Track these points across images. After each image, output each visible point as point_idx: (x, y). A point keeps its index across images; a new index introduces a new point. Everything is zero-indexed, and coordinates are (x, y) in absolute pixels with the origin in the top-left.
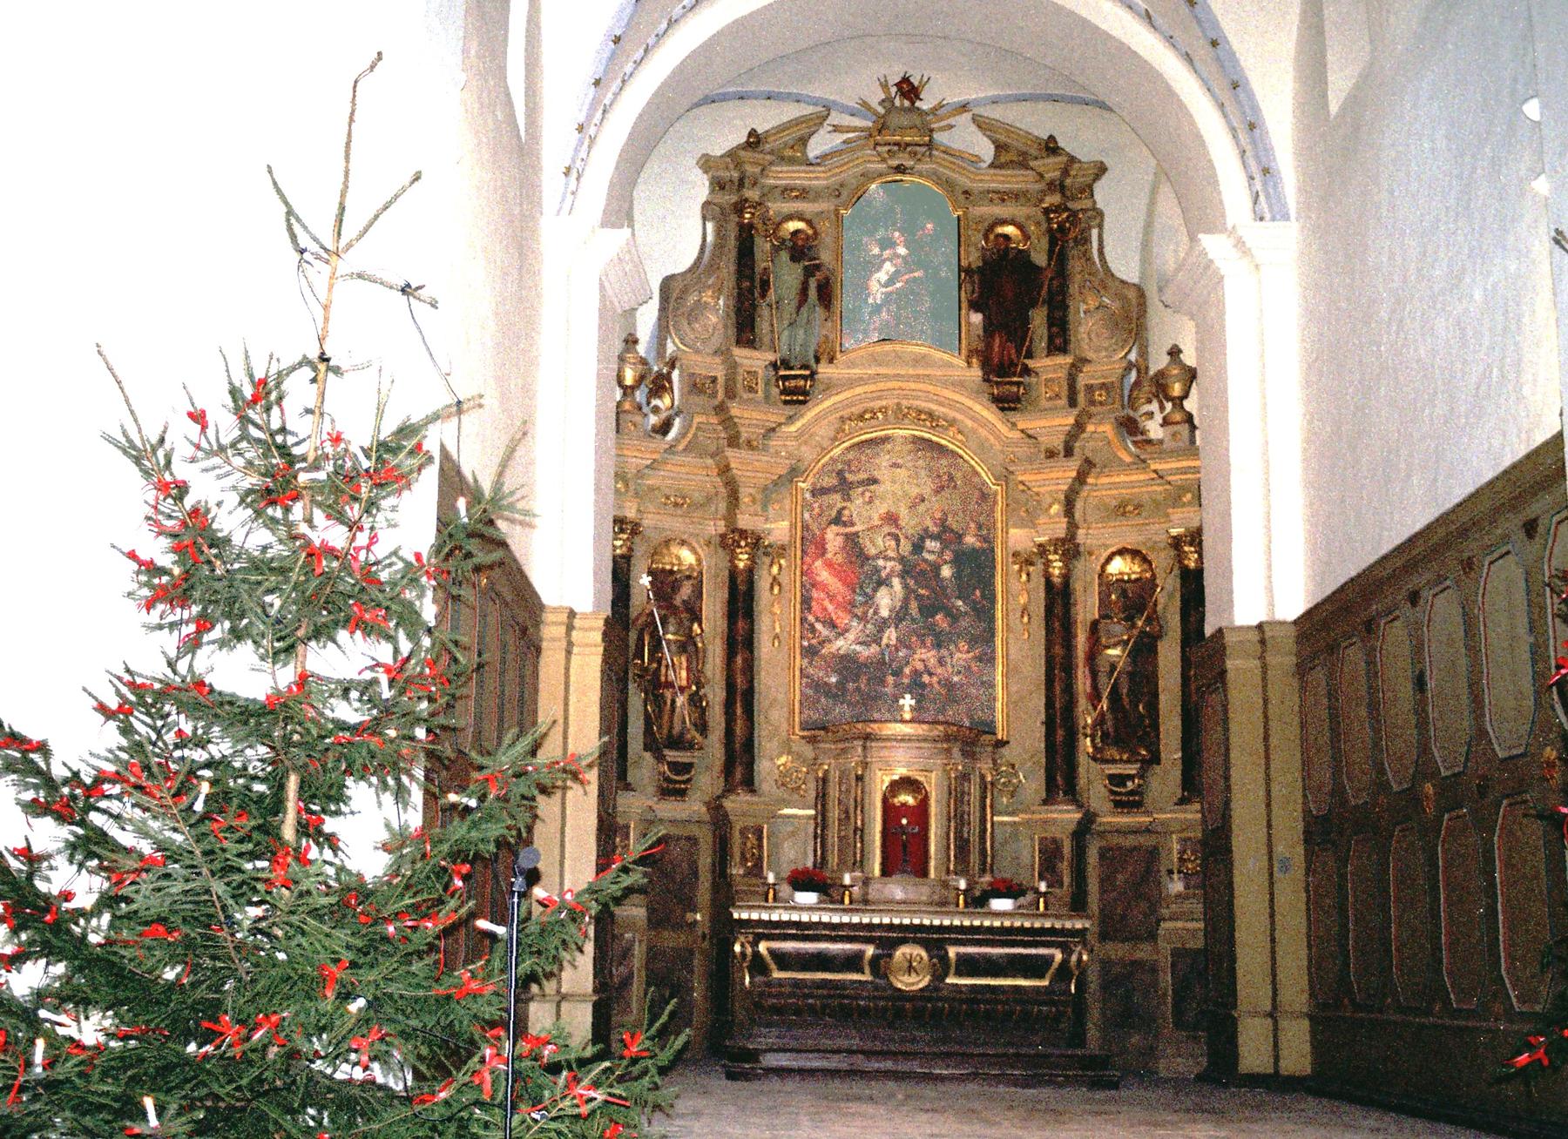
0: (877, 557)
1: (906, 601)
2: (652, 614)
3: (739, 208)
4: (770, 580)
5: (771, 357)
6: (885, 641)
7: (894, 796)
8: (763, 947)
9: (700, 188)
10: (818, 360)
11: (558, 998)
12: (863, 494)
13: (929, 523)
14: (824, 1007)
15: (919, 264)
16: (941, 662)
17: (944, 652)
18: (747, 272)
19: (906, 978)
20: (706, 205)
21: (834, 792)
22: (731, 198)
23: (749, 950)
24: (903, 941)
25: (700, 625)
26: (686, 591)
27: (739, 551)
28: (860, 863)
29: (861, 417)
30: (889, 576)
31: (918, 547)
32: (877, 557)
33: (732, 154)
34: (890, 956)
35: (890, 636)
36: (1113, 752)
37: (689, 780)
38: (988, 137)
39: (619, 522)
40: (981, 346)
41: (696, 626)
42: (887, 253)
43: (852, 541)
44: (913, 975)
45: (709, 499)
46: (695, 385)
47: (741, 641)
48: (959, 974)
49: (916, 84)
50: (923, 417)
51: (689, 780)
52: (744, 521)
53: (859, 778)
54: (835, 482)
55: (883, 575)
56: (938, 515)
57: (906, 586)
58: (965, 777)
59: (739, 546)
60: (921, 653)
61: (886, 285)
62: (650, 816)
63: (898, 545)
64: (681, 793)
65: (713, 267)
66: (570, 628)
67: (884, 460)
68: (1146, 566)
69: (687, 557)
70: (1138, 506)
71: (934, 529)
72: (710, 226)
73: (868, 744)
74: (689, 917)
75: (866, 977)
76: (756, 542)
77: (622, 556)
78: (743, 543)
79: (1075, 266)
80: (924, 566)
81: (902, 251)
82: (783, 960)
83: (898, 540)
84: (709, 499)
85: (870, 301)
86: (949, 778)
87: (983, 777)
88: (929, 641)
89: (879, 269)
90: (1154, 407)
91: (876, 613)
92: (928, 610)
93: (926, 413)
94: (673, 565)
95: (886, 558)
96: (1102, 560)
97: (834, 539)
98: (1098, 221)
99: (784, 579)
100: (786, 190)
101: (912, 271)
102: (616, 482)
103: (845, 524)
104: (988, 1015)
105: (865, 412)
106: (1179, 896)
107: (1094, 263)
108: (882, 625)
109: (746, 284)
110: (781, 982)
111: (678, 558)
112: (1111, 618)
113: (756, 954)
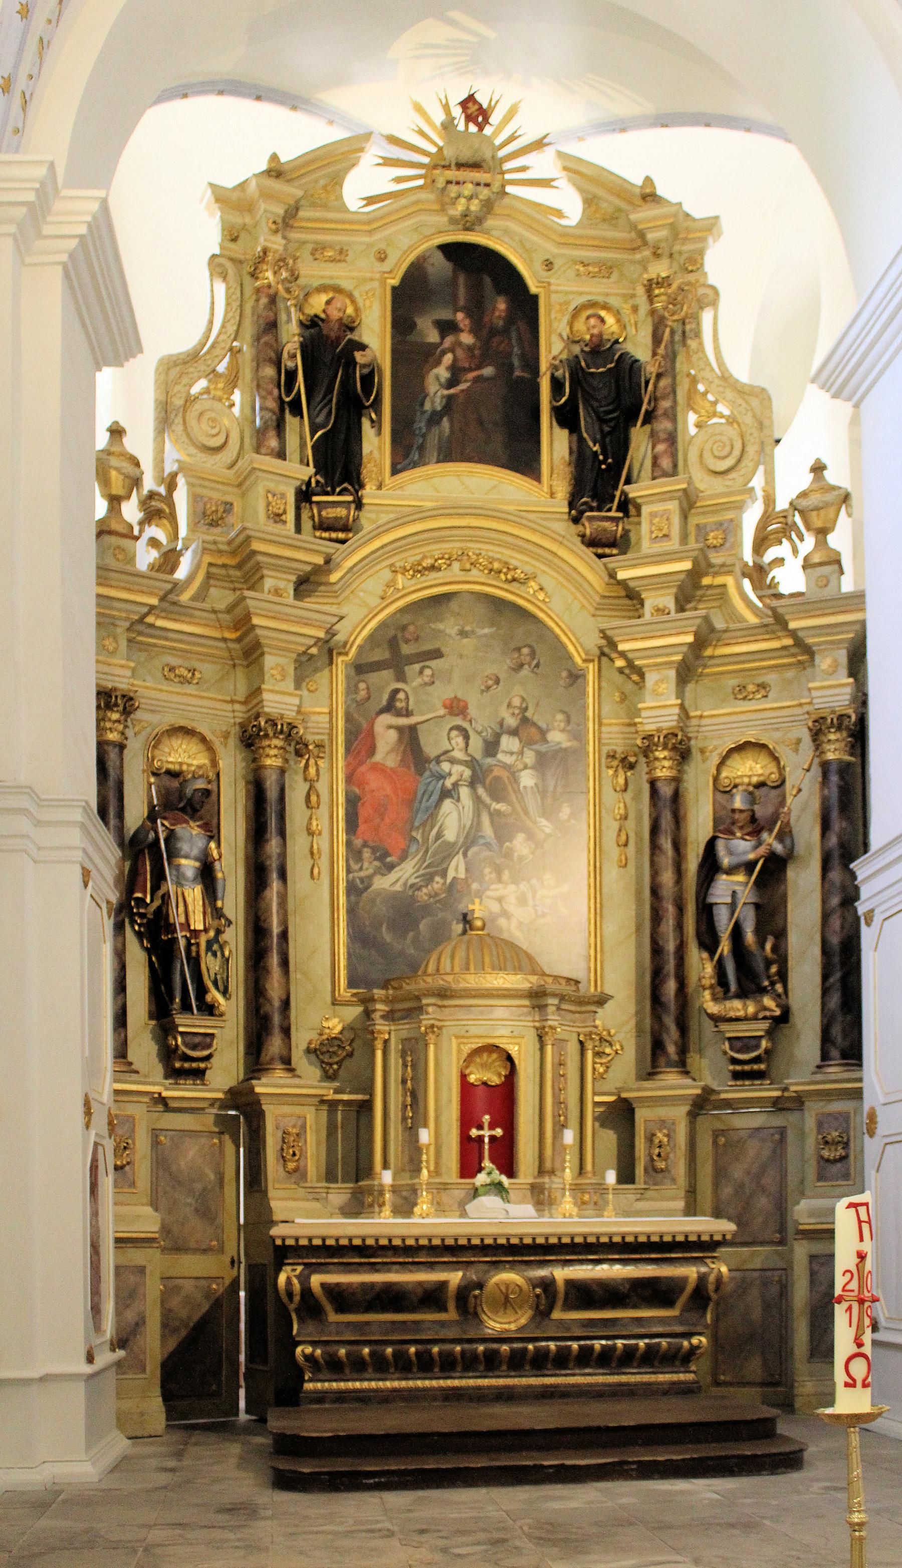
8: (316, 1280)
12: (421, 672)
17: (523, 886)
23: (297, 1286)
25: (219, 846)
30: (455, 785)
37: (208, 1058)
41: (213, 845)
42: (449, 341)
48: (569, 1306)
49: (485, 106)
51: (208, 1058)
54: (387, 655)
55: (449, 783)
57: (477, 799)
67: (449, 626)
81: (467, 339)
82: (338, 1295)
83: (467, 737)
85: (427, 406)
89: (438, 363)
91: (439, 836)
95: (453, 761)
101: (479, 367)
103: (398, 714)
113: (307, 1292)
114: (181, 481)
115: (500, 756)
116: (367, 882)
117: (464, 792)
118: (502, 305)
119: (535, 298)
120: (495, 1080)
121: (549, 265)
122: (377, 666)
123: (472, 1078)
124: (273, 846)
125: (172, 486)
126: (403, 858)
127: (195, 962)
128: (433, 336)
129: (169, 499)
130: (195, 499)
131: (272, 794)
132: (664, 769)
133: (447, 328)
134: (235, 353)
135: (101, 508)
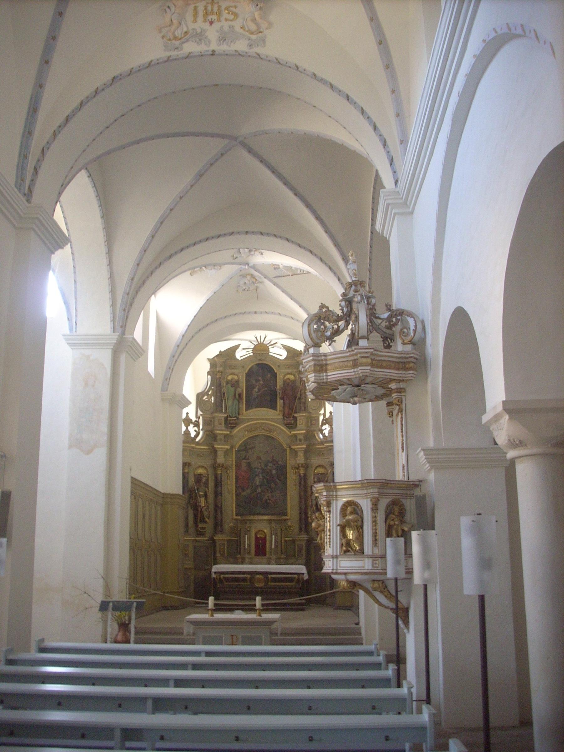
13: (269, 458)
30: (259, 473)
31: (266, 465)
35: (259, 490)
43: (249, 464)
47: (217, 494)
55: (257, 473)
81: (261, 382)
89: (255, 388)
95: (258, 469)
113: (220, 578)
114: (201, 417)
115: (268, 467)
116: (240, 493)
117: (261, 475)
118: (269, 375)
119: (276, 373)
120: (263, 536)
121: (279, 366)
122: (242, 451)
123: (258, 536)
124: (219, 489)
125: (199, 418)
126: (248, 488)
127: (201, 512)
128: (254, 382)
129: (198, 422)
130: (204, 420)
131: (219, 477)
132: (302, 471)
133: (257, 381)
134: (212, 389)
135: (184, 428)
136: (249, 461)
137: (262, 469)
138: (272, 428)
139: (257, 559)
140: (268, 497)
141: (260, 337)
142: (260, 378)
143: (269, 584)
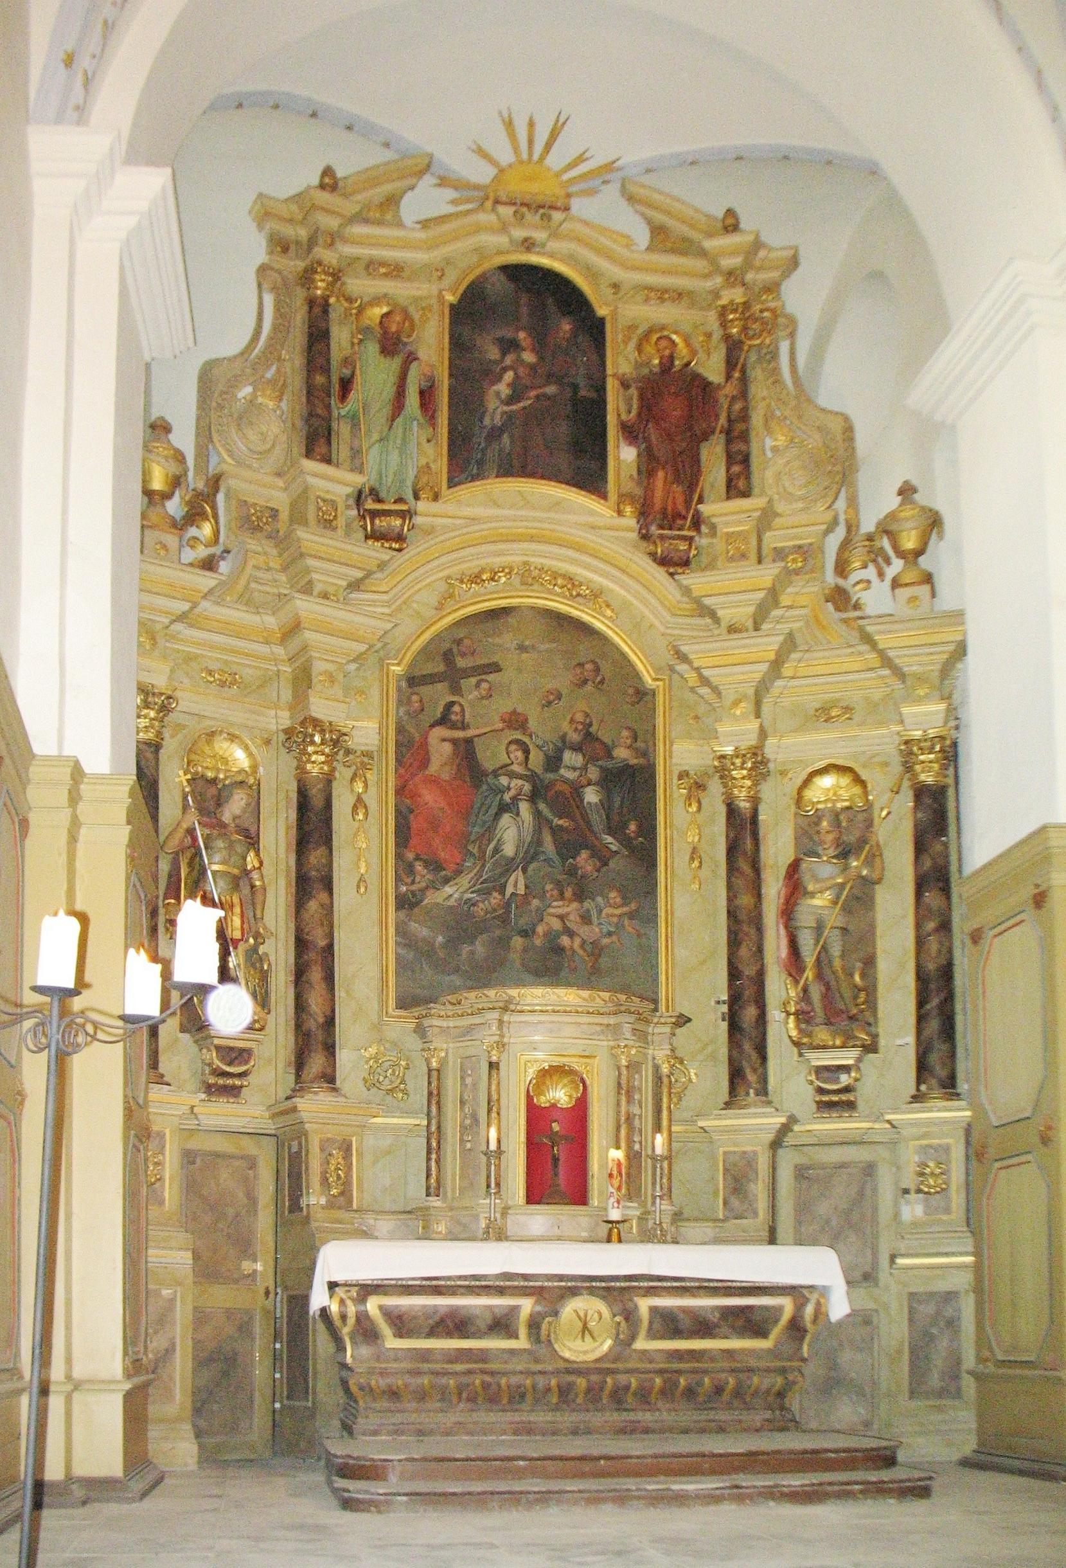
0: (496, 773)
1: (538, 831)
2: (191, 832)
3: (307, 277)
4: (352, 800)
5: (358, 480)
6: (510, 890)
7: (541, 1093)
8: (373, 1305)
9: (257, 250)
10: (417, 497)
11: (70, 1387)
12: (478, 685)
13: (566, 726)
14: (460, 1390)
15: (550, 378)
16: (586, 919)
18: (321, 361)
19: (578, 1344)
20: (262, 270)
21: (452, 1088)
22: (294, 265)
23: (351, 1309)
24: (574, 1292)
26: (236, 805)
27: (310, 749)
28: (495, 1185)
29: (476, 579)
30: (515, 799)
31: (553, 762)
32: (496, 773)
33: (297, 198)
34: (556, 1314)
35: (516, 883)
36: (822, 1034)
38: (642, 215)
39: (145, 691)
40: (638, 491)
43: (466, 752)
44: (588, 1337)
45: (265, 682)
46: (248, 518)
48: (652, 1335)
50: (560, 581)
52: (320, 707)
53: (493, 1066)
54: (441, 668)
55: (507, 797)
56: (579, 717)
57: (537, 814)
58: (634, 1066)
59: (313, 743)
60: (558, 907)
61: (510, 401)
62: (191, 1124)
63: (527, 759)
64: (233, 1092)
65: (272, 352)
66: (74, 798)
67: (508, 640)
68: (857, 790)
69: (240, 757)
70: (848, 709)
71: (574, 737)
72: (269, 300)
73: (506, 1018)
74: (247, 1266)
75: (522, 1342)
76: (337, 741)
77: (148, 743)
78: (317, 739)
79: (759, 390)
80: (559, 787)
81: (529, 357)
82: (401, 1324)
83: (527, 752)
84: (265, 682)
85: (487, 421)
86: (619, 1068)
87: (656, 1068)
88: (568, 893)
89: (499, 379)
90: (871, 572)
91: (497, 850)
92: (568, 848)
93: (564, 576)
94: (218, 770)
95: (512, 775)
96: (799, 782)
97: (440, 750)
98: (788, 331)
99: (371, 799)
100: (371, 266)
102: (140, 635)
103: (454, 726)
104: (690, 1393)
105: (482, 571)
106: (915, 1224)
107: (785, 387)
108: (509, 866)
109: (319, 379)
110: (398, 1356)
111: (225, 761)
112: (819, 856)
113: (362, 1319)
115: (562, 771)
117: (524, 807)
122: (431, 679)
128: (493, 353)
133: (509, 346)
136: (469, 733)
137: (532, 778)
138: (687, 1416)
139: (540, 1219)
140: (562, 918)
141: (531, 124)
142: (522, 335)
143: (641, 1344)
